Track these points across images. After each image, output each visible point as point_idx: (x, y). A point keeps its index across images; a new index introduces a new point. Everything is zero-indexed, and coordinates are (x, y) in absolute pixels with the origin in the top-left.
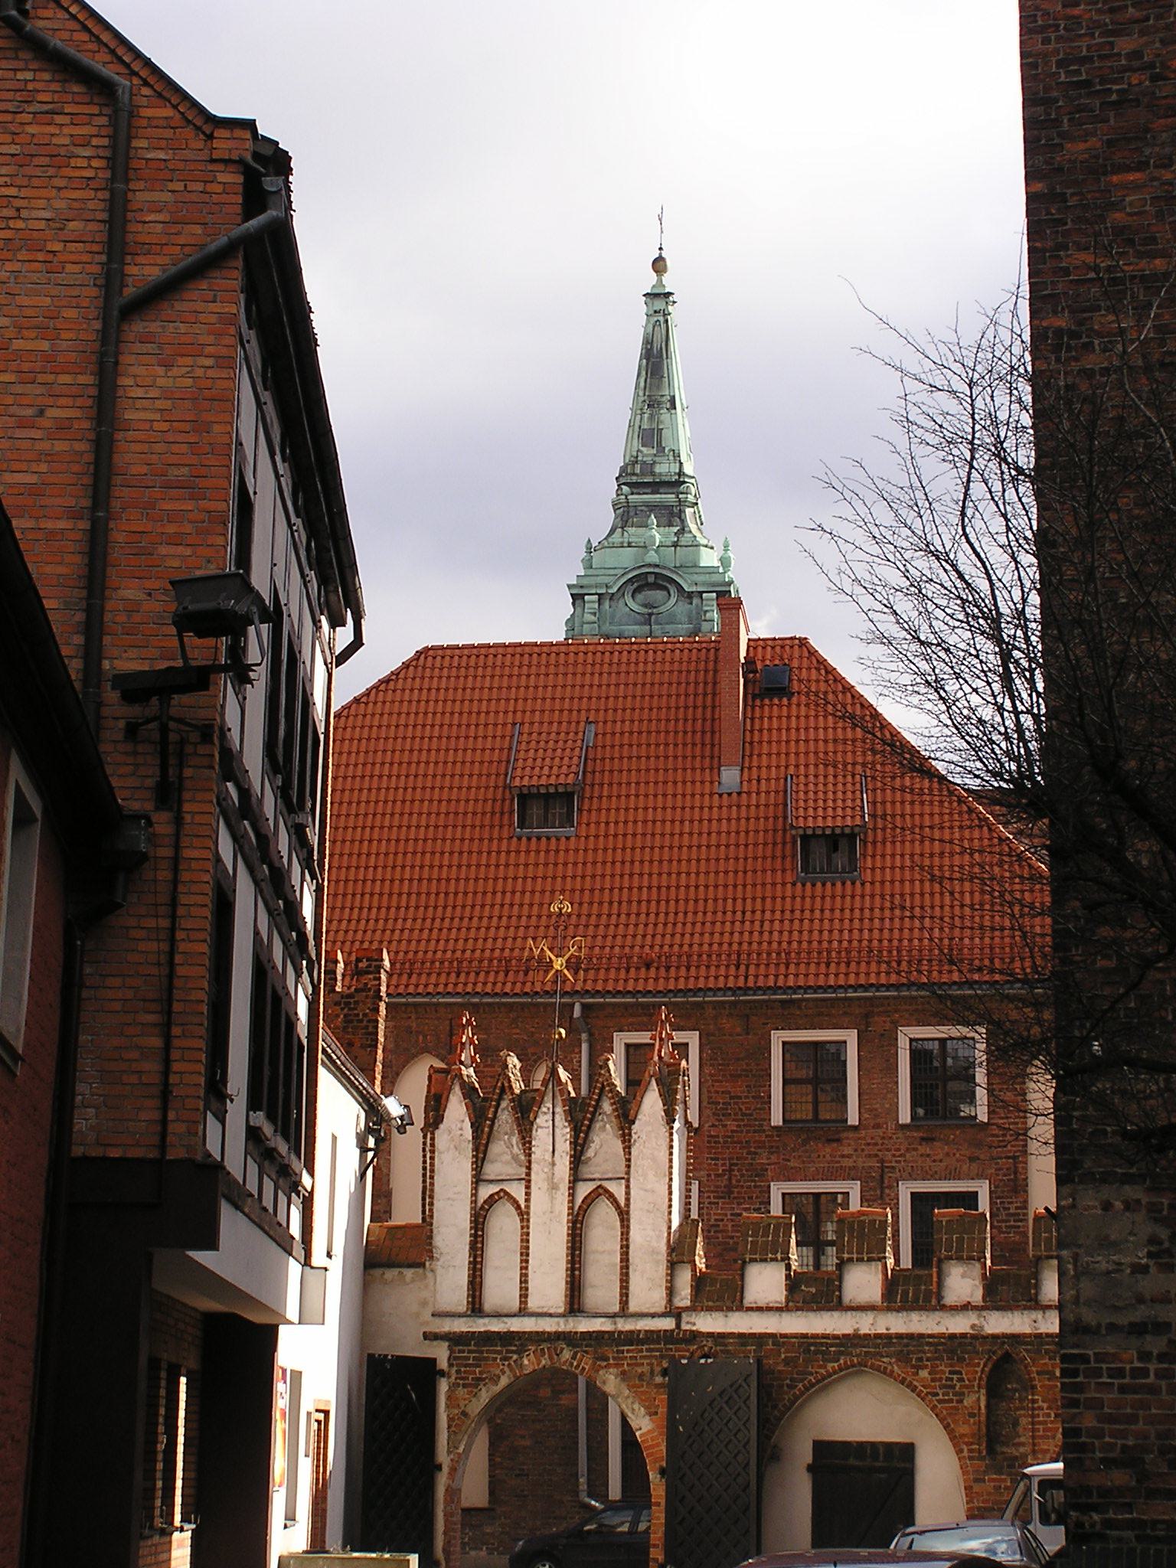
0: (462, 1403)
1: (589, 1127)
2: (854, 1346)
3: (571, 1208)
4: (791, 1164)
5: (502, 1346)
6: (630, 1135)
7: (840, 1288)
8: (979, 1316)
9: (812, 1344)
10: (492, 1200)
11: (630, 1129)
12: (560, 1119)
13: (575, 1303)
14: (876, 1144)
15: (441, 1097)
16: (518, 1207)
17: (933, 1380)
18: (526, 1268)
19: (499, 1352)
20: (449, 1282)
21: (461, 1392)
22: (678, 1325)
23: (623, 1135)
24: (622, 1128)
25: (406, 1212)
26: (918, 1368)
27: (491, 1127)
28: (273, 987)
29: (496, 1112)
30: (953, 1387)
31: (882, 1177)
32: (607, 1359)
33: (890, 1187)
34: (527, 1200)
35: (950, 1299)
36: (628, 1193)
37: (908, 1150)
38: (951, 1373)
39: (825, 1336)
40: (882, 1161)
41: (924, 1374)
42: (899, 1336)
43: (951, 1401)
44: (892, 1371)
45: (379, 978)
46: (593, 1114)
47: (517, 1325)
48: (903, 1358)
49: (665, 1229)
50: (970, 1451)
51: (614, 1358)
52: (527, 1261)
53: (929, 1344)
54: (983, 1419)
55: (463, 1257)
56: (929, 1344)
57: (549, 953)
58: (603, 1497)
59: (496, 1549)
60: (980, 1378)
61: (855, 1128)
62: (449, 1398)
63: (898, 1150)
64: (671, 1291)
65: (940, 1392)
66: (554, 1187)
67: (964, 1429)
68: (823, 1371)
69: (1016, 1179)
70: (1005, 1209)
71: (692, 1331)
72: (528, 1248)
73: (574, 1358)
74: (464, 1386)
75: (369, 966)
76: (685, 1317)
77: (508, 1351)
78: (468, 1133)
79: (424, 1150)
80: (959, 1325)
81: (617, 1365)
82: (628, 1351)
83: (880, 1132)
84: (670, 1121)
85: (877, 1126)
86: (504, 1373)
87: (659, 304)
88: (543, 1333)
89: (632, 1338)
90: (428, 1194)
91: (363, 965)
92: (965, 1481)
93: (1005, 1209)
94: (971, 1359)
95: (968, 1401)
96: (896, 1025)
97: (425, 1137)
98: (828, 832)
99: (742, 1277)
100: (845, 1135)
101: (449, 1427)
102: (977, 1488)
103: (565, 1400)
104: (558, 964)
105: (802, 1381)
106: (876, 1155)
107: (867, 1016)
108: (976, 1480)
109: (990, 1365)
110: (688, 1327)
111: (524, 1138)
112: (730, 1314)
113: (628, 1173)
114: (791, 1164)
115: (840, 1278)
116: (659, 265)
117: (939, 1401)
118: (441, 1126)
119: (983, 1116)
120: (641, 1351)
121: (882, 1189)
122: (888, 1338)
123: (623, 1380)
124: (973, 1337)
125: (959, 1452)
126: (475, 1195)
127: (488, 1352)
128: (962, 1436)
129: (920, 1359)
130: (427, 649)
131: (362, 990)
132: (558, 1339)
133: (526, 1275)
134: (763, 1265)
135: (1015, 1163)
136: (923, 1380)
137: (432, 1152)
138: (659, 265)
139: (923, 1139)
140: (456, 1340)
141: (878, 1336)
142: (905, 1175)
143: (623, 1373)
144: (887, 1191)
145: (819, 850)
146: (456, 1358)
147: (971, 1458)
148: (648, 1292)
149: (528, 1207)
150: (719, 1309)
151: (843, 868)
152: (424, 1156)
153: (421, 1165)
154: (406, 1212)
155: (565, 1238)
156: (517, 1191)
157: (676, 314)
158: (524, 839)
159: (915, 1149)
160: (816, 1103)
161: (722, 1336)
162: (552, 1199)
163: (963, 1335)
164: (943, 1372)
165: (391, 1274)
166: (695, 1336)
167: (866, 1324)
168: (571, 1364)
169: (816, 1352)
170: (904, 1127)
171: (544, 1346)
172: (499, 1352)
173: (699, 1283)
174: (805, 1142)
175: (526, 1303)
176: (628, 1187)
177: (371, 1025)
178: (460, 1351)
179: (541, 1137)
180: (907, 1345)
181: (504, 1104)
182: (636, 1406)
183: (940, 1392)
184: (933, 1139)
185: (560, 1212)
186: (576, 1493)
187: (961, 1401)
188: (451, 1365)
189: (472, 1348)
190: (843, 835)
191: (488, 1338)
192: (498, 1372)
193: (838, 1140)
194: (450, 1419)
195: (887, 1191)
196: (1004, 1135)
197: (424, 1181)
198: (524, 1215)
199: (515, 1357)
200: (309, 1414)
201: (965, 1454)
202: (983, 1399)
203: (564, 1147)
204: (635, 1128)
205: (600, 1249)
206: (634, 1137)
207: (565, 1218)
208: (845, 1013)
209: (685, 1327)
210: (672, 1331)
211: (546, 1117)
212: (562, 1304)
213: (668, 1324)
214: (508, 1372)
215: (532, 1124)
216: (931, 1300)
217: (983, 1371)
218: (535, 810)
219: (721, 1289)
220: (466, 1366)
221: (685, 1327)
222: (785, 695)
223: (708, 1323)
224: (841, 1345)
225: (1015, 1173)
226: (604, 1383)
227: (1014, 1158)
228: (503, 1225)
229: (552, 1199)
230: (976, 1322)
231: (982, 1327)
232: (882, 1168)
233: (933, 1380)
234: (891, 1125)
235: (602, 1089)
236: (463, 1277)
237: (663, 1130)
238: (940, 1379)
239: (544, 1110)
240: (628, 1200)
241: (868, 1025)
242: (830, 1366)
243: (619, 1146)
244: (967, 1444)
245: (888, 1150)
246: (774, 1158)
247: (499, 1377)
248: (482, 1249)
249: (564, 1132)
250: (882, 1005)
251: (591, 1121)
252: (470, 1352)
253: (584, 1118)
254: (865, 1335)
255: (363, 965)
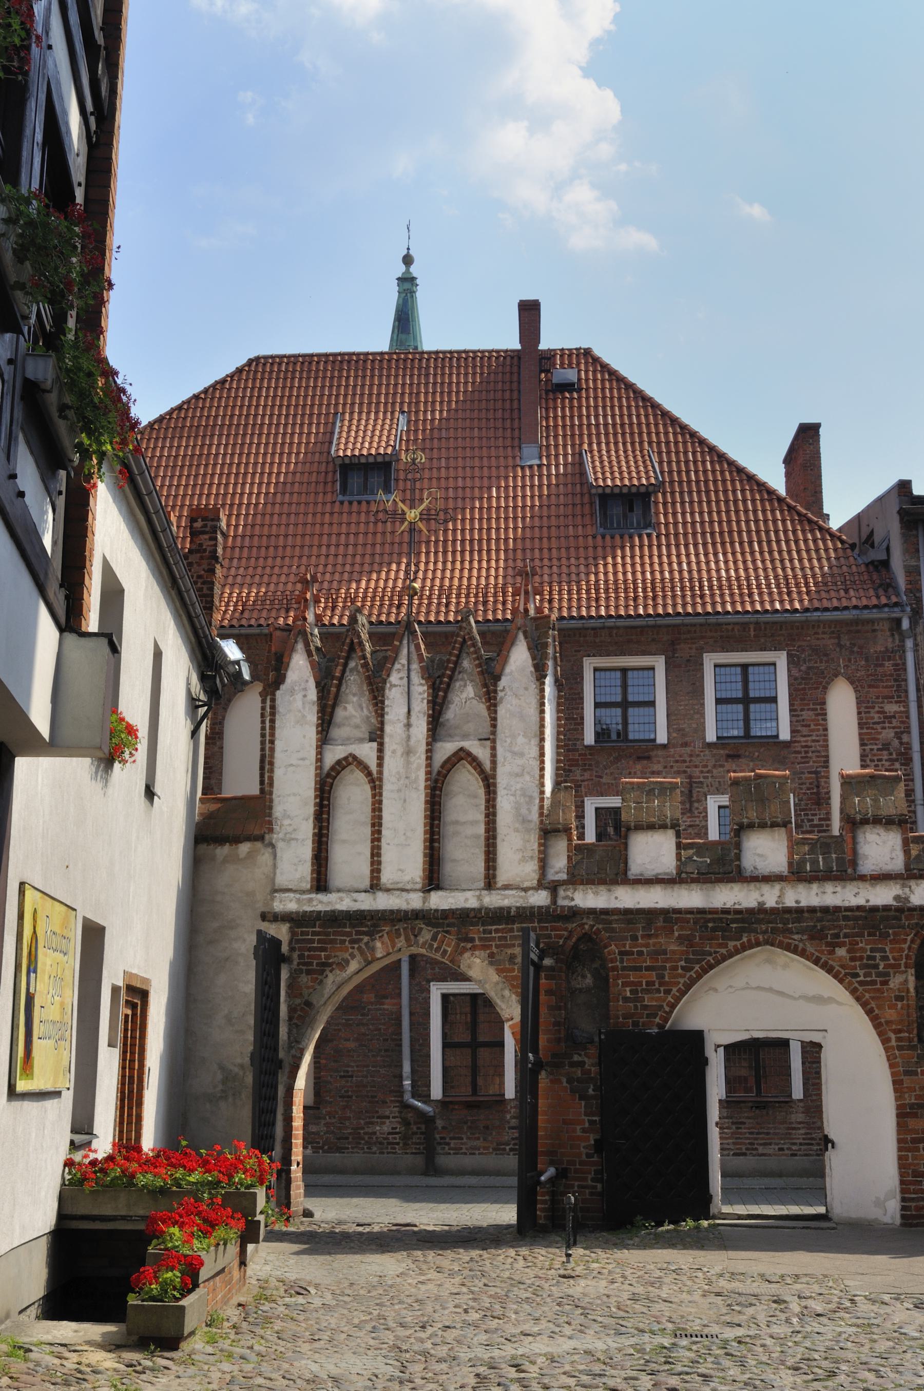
0: (305, 992)
1: (449, 685)
2: (760, 922)
3: (428, 773)
4: (604, 780)
5: (353, 926)
6: (495, 691)
7: (738, 857)
8: (903, 886)
9: (709, 920)
10: (341, 765)
11: (495, 685)
12: (416, 678)
13: (434, 878)
14: (685, 761)
15: (282, 656)
16: (369, 774)
17: (853, 959)
18: (379, 840)
19: (349, 934)
20: (293, 860)
21: (304, 979)
22: (554, 900)
23: (488, 693)
24: (485, 685)
25: (240, 781)
26: (834, 945)
27: (339, 686)
28: (108, 570)
29: (343, 672)
30: (876, 966)
31: (690, 791)
32: (472, 940)
33: (699, 801)
34: (380, 765)
35: (867, 866)
36: (494, 756)
37: (715, 766)
38: (872, 950)
39: (726, 911)
40: (690, 777)
41: (841, 952)
42: (812, 910)
43: (873, 983)
44: (804, 950)
45: (216, 539)
46: (453, 670)
47: (366, 902)
48: (816, 935)
49: (536, 795)
50: (899, 1039)
51: (481, 939)
52: (379, 832)
53: (846, 918)
54: (912, 1003)
55: (306, 829)
56: (846, 918)
57: (401, 505)
58: (425, 1097)
59: (322, 1148)
60: (907, 957)
61: (664, 746)
62: (290, 987)
63: (706, 766)
64: (543, 864)
65: (861, 973)
66: (409, 752)
67: (890, 1014)
68: (724, 951)
69: (818, 793)
70: (809, 820)
71: (570, 908)
72: (380, 817)
73: (434, 938)
74: (308, 972)
75: (205, 526)
76: (561, 893)
77: (358, 933)
78: (313, 694)
79: (263, 715)
80: (882, 896)
81: (484, 947)
82: (497, 931)
83: (688, 749)
84: (540, 677)
85: (685, 744)
86: (353, 956)
87: (407, 285)
88: (399, 911)
89: (500, 916)
90: (266, 763)
91: (198, 524)
92: (893, 1074)
93: (809, 820)
94: (895, 934)
95: (895, 982)
96: (701, 651)
97: (264, 701)
98: (625, 490)
99: (626, 846)
100: (655, 752)
101: (290, 1019)
102: (907, 1081)
103: (388, 1005)
104: (412, 515)
105: (698, 961)
106: (685, 772)
107: (673, 643)
108: (906, 1073)
109: (918, 941)
110: (566, 903)
111: (375, 698)
112: (613, 888)
113: (494, 733)
114: (604, 780)
115: (738, 846)
116: (408, 260)
117: (861, 983)
118: (283, 687)
119: (785, 735)
120: (512, 930)
121: (691, 803)
122: (799, 912)
123: (491, 963)
124: (899, 910)
125: (885, 1041)
126: (320, 760)
127: (335, 933)
128: (888, 1023)
129: (837, 936)
130: (257, 359)
131: (198, 551)
132: (417, 918)
133: (379, 848)
134: (650, 833)
135: (817, 778)
136: (840, 959)
137: (273, 714)
138: (408, 260)
139: (728, 756)
140: (297, 920)
141: (788, 910)
142: (712, 789)
143: (491, 955)
144: (696, 805)
145: (617, 510)
146: (298, 941)
147: (900, 1048)
148: (517, 861)
149: (380, 772)
150: (602, 882)
151: (638, 524)
152: (263, 722)
153: (259, 739)
154: (240, 781)
155: (423, 806)
156: (367, 752)
157: (422, 295)
158: (346, 504)
159: (722, 766)
160: (625, 723)
161: (605, 912)
162: (408, 763)
163: (886, 908)
164: (863, 950)
165: (223, 851)
166: (575, 913)
167: (770, 896)
168: (431, 946)
169: (714, 929)
170: (710, 745)
171: (400, 926)
172: (349, 934)
173: (579, 852)
174: (618, 759)
175: (379, 878)
176: (494, 748)
177: (205, 587)
178: (303, 933)
179: (395, 698)
180: (820, 920)
181: (352, 664)
182: (507, 993)
183: (861, 973)
184: (738, 756)
185: (417, 778)
186: (400, 1091)
187: (885, 983)
188: (292, 949)
189: (317, 929)
190: (638, 494)
191: (334, 919)
192: (347, 956)
193: (648, 758)
194: (292, 1010)
195: (696, 805)
196: (806, 752)
197: (263, 749)
198: (376, 783)
199: (366, 939)
200: (115, 990)
201: (893, 1043)
202: (912, 980)
203: (421, 706)
204: (503, 683)
205: (462, 818)
206: (500, 694)
207: (422, 784)
208: (653, 640)
209: (561, 902)
210: (548, 907)
211: (400, 675)
212: (418, 880)
213: (540, 898)
214: (358, 957)
215: (385, 681)
216: (846, 870)
217: (910, 948)
218: (355, 481)
219: (606, 860)
220: (309, 950)
221: (561, 902)
222: (575, 390)
223: (589, 899)
224: (743, 921)
225: (818, 787)
226: (469, 967)
227: (816, 773)
228: (353, 795)
229: (408, 763)
230: (900, 892)
231: (907, 899)
232: (691, 783)
233: (853, 959)
234: (698, 744)
235: (464, 641)
236: (306, 851)
237: (533, 687)
238: (861, 958)
239: (397, 666)
240: (494, 762)
241: (674, 651)
242: (731, 944)
243: (481, 708)
244: (896, 1032)
245: (696, 766)
246: (587, 775)
247: (347, 962)
248: (328, 820)
249: (421, 690)
250: (689, 632)
251: (451, 678)
252: (314, 933)
253: (443, 675)
254: (772, 909)
255: (198, 524)
